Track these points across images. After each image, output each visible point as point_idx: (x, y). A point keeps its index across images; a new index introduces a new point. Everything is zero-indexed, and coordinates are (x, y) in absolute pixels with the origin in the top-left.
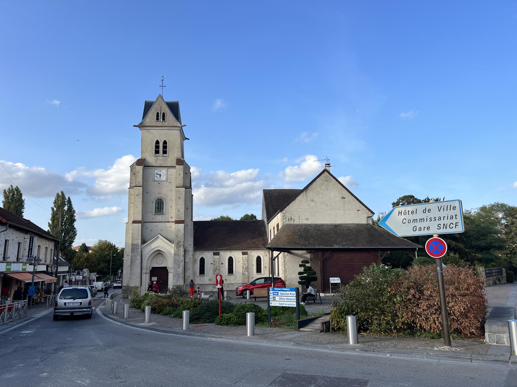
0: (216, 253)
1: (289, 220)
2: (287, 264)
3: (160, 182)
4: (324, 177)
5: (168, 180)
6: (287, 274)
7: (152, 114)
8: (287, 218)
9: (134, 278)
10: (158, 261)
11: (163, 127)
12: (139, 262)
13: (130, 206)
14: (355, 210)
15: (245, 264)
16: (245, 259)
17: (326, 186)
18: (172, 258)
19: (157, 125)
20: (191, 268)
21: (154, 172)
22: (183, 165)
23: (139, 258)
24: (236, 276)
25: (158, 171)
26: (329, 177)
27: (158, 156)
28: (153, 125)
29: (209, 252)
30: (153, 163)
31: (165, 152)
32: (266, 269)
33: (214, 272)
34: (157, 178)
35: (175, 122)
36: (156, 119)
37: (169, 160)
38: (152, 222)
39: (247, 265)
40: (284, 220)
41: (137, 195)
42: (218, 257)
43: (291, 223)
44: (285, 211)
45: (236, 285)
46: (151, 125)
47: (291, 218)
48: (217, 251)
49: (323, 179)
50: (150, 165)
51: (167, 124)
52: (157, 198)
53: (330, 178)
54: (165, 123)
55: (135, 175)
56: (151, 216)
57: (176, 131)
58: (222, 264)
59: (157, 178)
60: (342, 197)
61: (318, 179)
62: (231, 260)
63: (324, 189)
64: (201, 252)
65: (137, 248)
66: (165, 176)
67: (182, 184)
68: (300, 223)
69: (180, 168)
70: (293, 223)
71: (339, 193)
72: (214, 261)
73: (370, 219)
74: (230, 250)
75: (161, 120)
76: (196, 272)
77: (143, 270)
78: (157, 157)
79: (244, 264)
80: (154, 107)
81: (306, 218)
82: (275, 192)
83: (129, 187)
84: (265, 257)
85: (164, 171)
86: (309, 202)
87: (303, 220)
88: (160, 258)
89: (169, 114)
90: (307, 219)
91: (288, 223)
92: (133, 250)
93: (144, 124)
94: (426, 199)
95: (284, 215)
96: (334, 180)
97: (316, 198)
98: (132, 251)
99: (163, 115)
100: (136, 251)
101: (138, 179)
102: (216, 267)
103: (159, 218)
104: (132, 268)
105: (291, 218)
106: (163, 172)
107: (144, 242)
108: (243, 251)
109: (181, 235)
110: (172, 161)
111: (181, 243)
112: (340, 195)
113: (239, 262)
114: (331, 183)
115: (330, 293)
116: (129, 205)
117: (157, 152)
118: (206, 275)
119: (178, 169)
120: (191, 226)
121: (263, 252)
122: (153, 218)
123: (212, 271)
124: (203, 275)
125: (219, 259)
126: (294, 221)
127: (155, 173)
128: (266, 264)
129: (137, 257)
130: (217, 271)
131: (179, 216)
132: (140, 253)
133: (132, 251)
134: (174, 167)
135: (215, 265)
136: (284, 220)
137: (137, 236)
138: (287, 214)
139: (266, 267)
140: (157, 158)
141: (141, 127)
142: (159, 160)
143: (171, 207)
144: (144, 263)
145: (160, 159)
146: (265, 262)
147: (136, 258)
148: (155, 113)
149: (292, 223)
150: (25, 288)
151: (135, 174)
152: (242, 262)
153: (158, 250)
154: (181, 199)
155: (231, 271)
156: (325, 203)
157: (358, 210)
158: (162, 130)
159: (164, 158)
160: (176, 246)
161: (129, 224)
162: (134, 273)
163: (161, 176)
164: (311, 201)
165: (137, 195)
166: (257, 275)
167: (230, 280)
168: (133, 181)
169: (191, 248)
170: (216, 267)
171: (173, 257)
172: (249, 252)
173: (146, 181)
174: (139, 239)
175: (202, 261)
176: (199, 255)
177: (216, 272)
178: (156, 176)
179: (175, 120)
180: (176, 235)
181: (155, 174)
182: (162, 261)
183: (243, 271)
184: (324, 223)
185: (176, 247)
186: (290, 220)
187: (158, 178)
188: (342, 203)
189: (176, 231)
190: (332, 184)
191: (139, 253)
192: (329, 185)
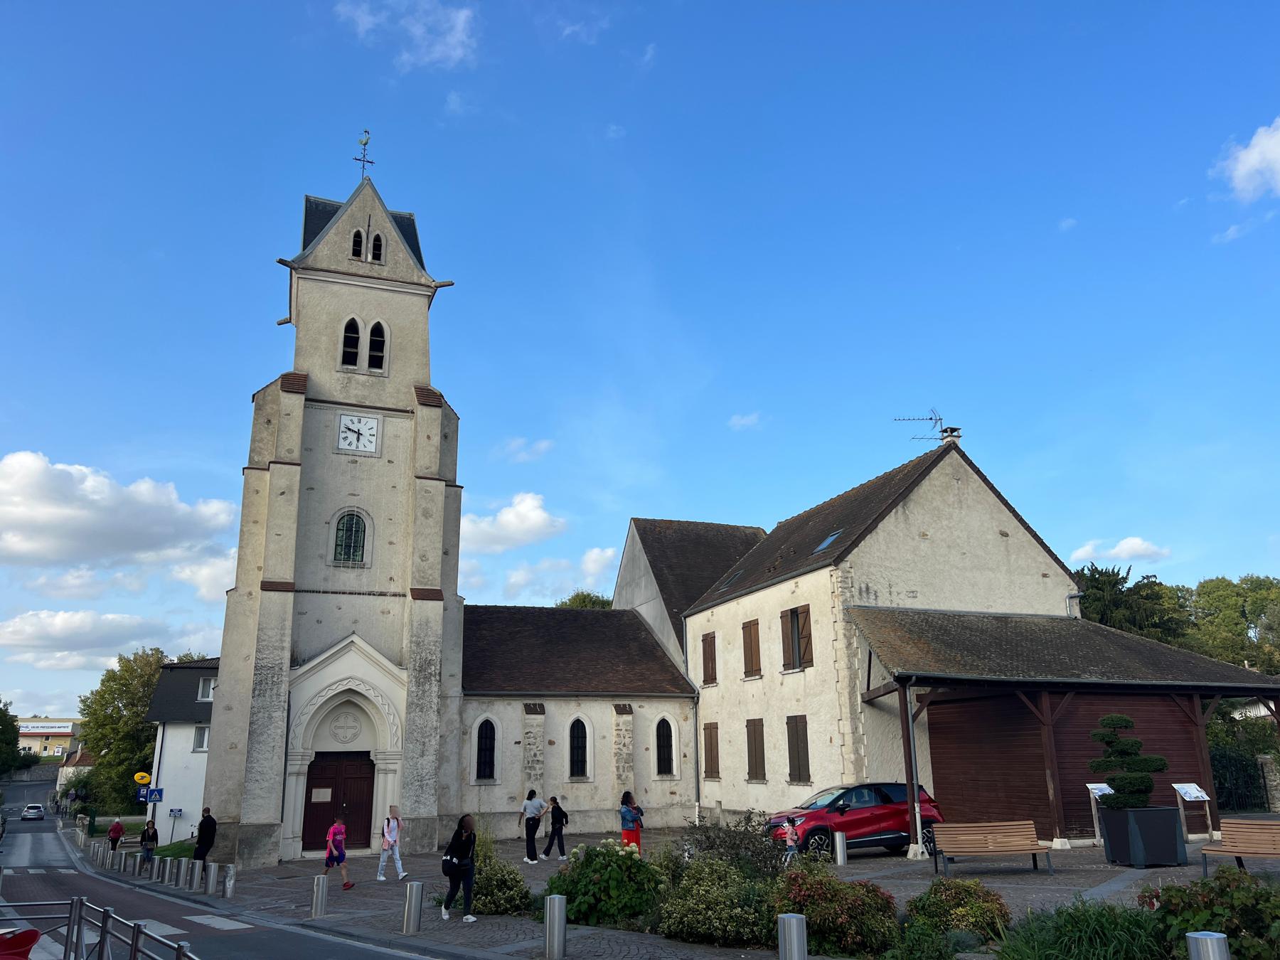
0: (535, 705)
1: (860, 593)
2: (863, 740)
3: (357, 458)
4: (951, 465)
5: (385, 452)
6: (865, 776)
7: (334, 243)
8: (857, 586)
9: (258, 791)
10: (340, 731)
11: (374, 278)
12: (279, 731)
14: (1038, 573)
15: (624, 745)
16: (624, 730)
17: (958, 494)
18: (397, 721)
19: (353, 270)
20: (451, 758)
21: (337, 421)
23: (280, 716)
24: (596, 784)
25: (351, 420)
26: (962, 466)
27: (353, 372)
28: (340, 269)
29: (509, 704)
30: (335, 394)
31: (376, 362)
32: (685, 762)
33: (528, 771)
34: (348, 442)
35: (413, 270)
36: (351, 252)
37: (390, 387)
38: (325, 592)
39: (631, 747)
40: (848, 595)
41: (283, 493)
42: (539, 718)
43: (867, 604)
44: (848, 564)
45: (595, 817)
46: (333, 268)
47: (868, 588)
48: (538, 701)
49: (947, 472)
50: (324, 399)
51: (389, 271)
52: (346, 510)
53: (965, 470)
54: (380, 267)
55: (270, 427)
56: (323, 572)
57: (415, 298)
58: (551, 743)
59: (348, 442)
60: (1001, 531)
61: (934, 471)
62: (578, 730)
63: (954, 502)
64: (484, 703)
65: (275, 679)
66: (373, 439)
67: (435, 469)
68: (894, 605)
69: (428, 415)
70: (874, 605)
71: (993, 518)
72: (527, 733)
73: (1075, 604)
74: (577, 696)
75: (370, 258)
76: (465, 770)
77: (289, 763)
78: (350, 375)
79: (621, 746)
80: (347, 212)
81: (908, 589)
82: (668, 528)
84: (682, 722)
85: (373, 423)
86: (913, 539)
87: (902, 596)
88: (347, 721)
89: (396, 242)
90: (913, 592)
91: (858, 602)
92: (258, 687)
93: (310, 262)
94: (1083, 569)
95: (847, 578)
96: (976, 477)
97: (934, 528)
98: (257, 692)
99: (374, 244)
100: (272, 690)
101: (284, 437)
102: (535, 755)
103: (348, 578)
104: (255, 754)
105: (868, 588)
106: (369, 424)
107: (295, 662)
108: (618, 703)
110: (398, 391)
111: (433, 668)
112: (994, 524)
113: (604, 737)
114: (970, 487)
115: (1094, 836)
116: (242, 526)
117: (350, 358)
118: (498, 782)
119: (423, 417)
120: (456, 610)
121: (677, 706)
122: (326, 579)
123: (518, 767)
124: (491, 781)
125: (544, 725)
126: (876, 597)
127: (342, 426)
128: (687, 745)
129: (274, 715)
130: (538, 766)
131: (422, 575)
132: (284, 698)
133: (254, 690)
135: (532, 746)
136: (848, 595)
137: (278, 637)
138: (855, 574)
139: (685, 756)
140: (348, 378)
141: (303, 269)
143: (391, 543)
144: (296, 737)
145: (360, 382)
146: (682, 740)
147: (270, 718)
148: (350, 232)
149: (872, 603)
150: (927, 850)
151: (269, 421)
152: (614, 739)
153: (350, 691)
154: (431, 516)
155: (578, 767)
156: (959, 545)
157: (1045, 576)
158: (365, 290)
159: (373, 379)
160: (415, 677)
161: (240, 595)
162: (261, 773)
163: (361, 437)
164: (919, 535)
165: (283, 493)
166: (659, 783)
167: (577, 797)
168: (260, 445)
169: (455, 687)
170: (535, 755)
171: (403, 715)
172: (635, 705)
173: (311, 450)
174: (283, 648)
175: (487, 731)
176: (478, 713)
177: (533, 773)
179: (415, 264)
181: (343, 429)
182: (353, 731)
183: (621, 770)
184: (960, 609)
185: (414, 680)
186: (864, 595)
187: (350, 444)
188: (1002, 549)
189: (415, 624)
190: (972, 488)
191: (282, 698)
192: (966, 491)
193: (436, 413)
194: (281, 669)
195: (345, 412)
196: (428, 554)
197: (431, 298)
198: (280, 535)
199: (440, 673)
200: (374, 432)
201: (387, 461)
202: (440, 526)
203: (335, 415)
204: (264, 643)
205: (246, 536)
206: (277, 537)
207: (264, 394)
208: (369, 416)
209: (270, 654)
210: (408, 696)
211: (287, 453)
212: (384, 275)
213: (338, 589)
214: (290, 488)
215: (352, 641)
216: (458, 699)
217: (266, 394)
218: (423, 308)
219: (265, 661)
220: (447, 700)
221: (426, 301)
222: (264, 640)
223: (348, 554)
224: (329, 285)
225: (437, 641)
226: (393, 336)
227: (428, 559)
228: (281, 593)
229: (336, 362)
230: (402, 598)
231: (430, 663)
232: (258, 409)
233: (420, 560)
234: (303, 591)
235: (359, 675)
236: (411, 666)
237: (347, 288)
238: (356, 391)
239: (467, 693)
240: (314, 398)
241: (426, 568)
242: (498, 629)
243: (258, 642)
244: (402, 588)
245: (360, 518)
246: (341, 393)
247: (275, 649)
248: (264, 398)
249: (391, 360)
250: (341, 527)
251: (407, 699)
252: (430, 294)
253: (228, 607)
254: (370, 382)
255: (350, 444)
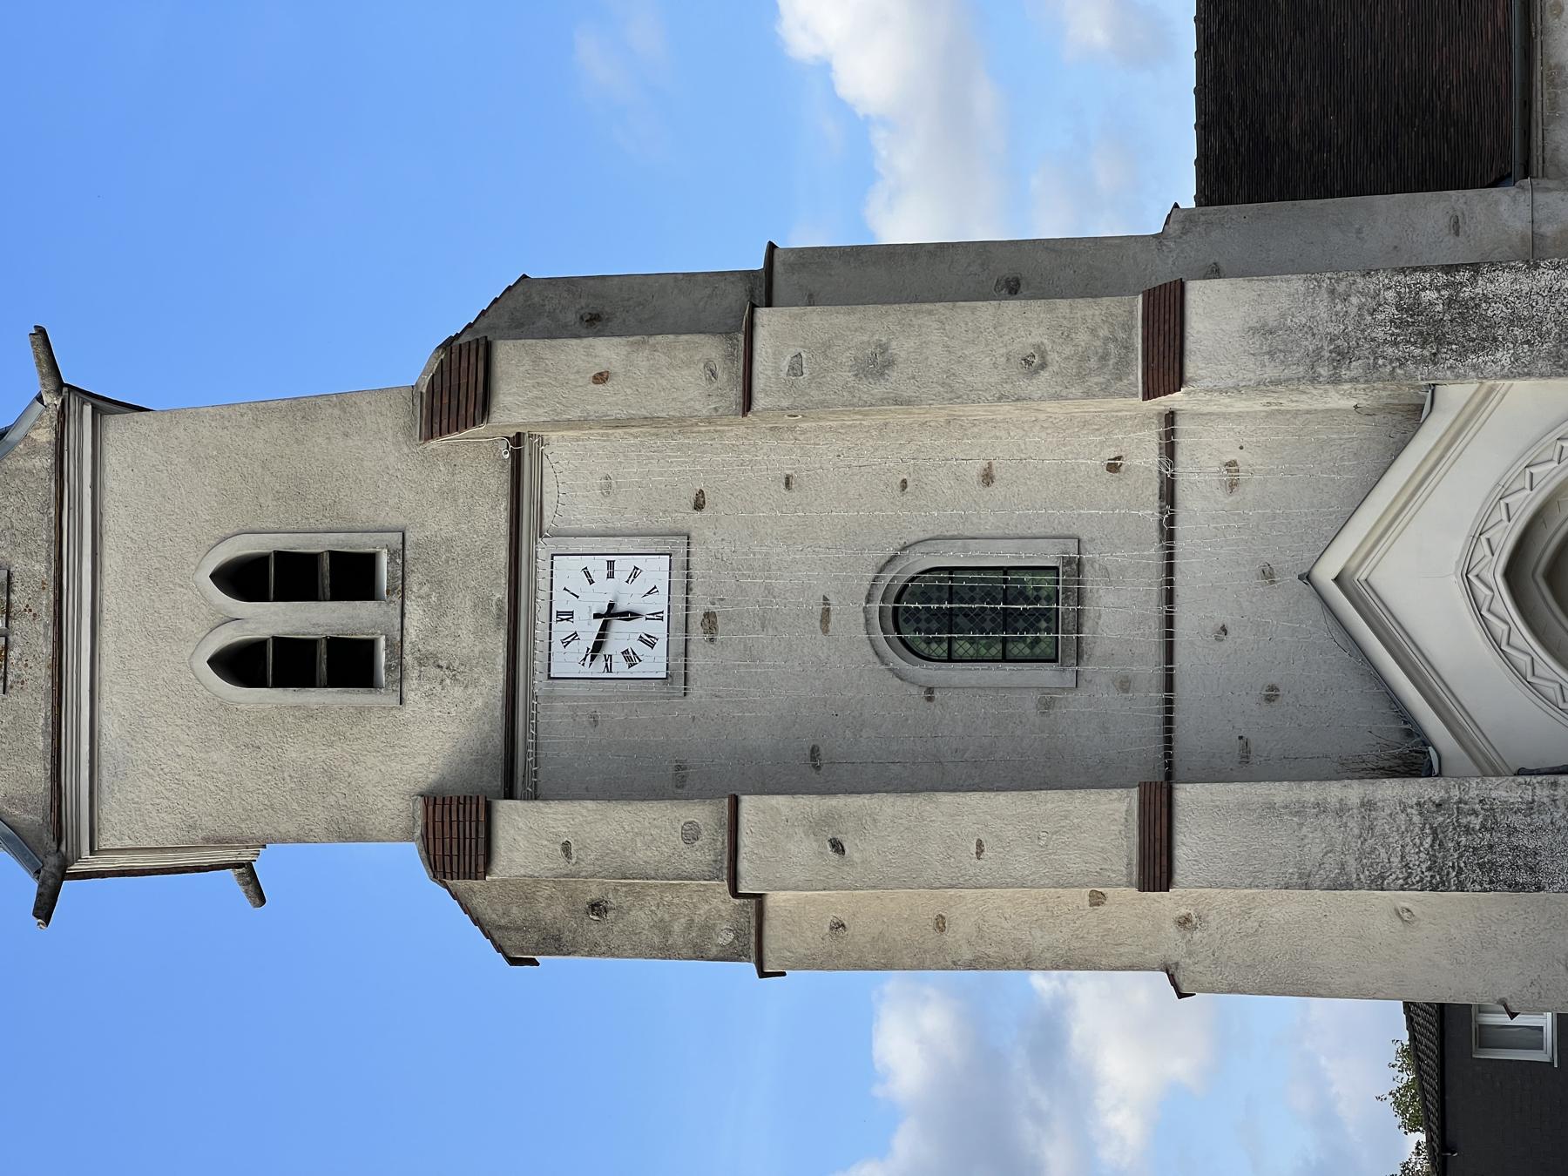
3: (697, 613)
11: (59, 601)
13: (967, 955)
22: (488, 347)
25: (566, 643)
27: (396, 649)
30: (479, 703)
34: (640, 649)
41: (837, 847)
46: (41, 743)
50: (498, 739)
54: (17, 587)
55: (613, 901)
57: (112, 459)
59: (640, 649)
64: (1554, 106)
65: (1476, 822)
66: (624, 565)
67: (711, 348)
78: (408, 659)
83: (751, 967)
85: (568, 571)
98: (1522, 878)
100: (1512, 831)
101: (643, 856)
109: (1322, 311)
122: (1125, 685)
127: (587, 671)
131: (1093, 363)
133: (1515, 887)
134: (517, 458)
142: (435, 630)
143: (988, 478)
153: (1513, 573)
154: (884, 348)
159: (413, 581)
160: (1462, 354)
161: (1190, 954)
163: (621, 606)
165: (837, 847)
168: (677, 927)
174: (1368, 805)
178: (620, 668)
180: (1324, 371)
185: (1472, 360)
187: (649, 642)
189: (1271, 372)
191: (1543, 794)
193: (510, 358)
194: (1439, 805)
195: (539, 665)
196: (1016, 347)
197: (104, 406)
198: (980, 844)
199: (1449, 269)
200: (598, 566)
201: (698, 514)
202: (916, 313)
203: (550, 697)
204: (1352, 865)
205: (991, 951)
206: (987, 853)
207: (506, 928)
208: (543, 584)
209: (1387, 846)
210: (1529, 374)
211: (697, 843)
212: (41, 568)
213: (1155, 654)
214: (815, 826)
215: (1337, 580)
216: (1539, 197)
217: (503, 922)
218: (144, 429)
219: (1412, 859)
220: (1543, 236)
221: (116, 427)
222: (1343, 866)
223: (1033, 620)
224: (106, 745)
225: (1332, 292)
226: (256, 526)
227: (1039, 348)
228: (1179, 826)
229: (370, 709)
230: (1181, 425)
231: (1411, 308)
232: (556, 944)
233: (1045, 374)
234: (1168, 756)
235: (1457, 546)
236: (1422, 375)
237: (105, 689)
238: (463, 633)
239: (1517, 169)
240: (501, 766)
241: (1069, 350)
242: (1284, 76)
243: (1348, 886)
244: (1143, 426)
245: (905, 587)
246: (475, 682)
247: (1371, 828)
248: (518, 929)
249: (345, 525)
250: (941, 650)
251: (1542, 375)
252: (88, 409)
253: (1233, 989)
254: (426, 589)
255: (649, 642)
